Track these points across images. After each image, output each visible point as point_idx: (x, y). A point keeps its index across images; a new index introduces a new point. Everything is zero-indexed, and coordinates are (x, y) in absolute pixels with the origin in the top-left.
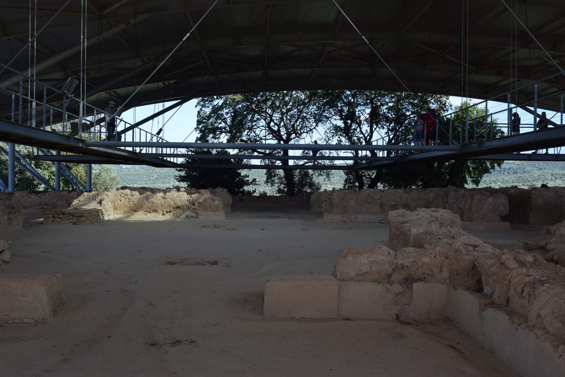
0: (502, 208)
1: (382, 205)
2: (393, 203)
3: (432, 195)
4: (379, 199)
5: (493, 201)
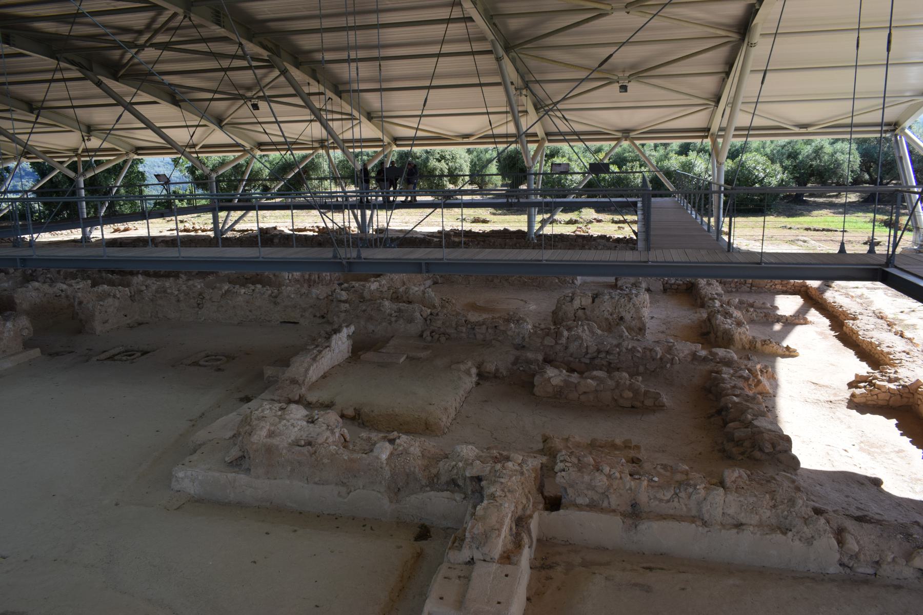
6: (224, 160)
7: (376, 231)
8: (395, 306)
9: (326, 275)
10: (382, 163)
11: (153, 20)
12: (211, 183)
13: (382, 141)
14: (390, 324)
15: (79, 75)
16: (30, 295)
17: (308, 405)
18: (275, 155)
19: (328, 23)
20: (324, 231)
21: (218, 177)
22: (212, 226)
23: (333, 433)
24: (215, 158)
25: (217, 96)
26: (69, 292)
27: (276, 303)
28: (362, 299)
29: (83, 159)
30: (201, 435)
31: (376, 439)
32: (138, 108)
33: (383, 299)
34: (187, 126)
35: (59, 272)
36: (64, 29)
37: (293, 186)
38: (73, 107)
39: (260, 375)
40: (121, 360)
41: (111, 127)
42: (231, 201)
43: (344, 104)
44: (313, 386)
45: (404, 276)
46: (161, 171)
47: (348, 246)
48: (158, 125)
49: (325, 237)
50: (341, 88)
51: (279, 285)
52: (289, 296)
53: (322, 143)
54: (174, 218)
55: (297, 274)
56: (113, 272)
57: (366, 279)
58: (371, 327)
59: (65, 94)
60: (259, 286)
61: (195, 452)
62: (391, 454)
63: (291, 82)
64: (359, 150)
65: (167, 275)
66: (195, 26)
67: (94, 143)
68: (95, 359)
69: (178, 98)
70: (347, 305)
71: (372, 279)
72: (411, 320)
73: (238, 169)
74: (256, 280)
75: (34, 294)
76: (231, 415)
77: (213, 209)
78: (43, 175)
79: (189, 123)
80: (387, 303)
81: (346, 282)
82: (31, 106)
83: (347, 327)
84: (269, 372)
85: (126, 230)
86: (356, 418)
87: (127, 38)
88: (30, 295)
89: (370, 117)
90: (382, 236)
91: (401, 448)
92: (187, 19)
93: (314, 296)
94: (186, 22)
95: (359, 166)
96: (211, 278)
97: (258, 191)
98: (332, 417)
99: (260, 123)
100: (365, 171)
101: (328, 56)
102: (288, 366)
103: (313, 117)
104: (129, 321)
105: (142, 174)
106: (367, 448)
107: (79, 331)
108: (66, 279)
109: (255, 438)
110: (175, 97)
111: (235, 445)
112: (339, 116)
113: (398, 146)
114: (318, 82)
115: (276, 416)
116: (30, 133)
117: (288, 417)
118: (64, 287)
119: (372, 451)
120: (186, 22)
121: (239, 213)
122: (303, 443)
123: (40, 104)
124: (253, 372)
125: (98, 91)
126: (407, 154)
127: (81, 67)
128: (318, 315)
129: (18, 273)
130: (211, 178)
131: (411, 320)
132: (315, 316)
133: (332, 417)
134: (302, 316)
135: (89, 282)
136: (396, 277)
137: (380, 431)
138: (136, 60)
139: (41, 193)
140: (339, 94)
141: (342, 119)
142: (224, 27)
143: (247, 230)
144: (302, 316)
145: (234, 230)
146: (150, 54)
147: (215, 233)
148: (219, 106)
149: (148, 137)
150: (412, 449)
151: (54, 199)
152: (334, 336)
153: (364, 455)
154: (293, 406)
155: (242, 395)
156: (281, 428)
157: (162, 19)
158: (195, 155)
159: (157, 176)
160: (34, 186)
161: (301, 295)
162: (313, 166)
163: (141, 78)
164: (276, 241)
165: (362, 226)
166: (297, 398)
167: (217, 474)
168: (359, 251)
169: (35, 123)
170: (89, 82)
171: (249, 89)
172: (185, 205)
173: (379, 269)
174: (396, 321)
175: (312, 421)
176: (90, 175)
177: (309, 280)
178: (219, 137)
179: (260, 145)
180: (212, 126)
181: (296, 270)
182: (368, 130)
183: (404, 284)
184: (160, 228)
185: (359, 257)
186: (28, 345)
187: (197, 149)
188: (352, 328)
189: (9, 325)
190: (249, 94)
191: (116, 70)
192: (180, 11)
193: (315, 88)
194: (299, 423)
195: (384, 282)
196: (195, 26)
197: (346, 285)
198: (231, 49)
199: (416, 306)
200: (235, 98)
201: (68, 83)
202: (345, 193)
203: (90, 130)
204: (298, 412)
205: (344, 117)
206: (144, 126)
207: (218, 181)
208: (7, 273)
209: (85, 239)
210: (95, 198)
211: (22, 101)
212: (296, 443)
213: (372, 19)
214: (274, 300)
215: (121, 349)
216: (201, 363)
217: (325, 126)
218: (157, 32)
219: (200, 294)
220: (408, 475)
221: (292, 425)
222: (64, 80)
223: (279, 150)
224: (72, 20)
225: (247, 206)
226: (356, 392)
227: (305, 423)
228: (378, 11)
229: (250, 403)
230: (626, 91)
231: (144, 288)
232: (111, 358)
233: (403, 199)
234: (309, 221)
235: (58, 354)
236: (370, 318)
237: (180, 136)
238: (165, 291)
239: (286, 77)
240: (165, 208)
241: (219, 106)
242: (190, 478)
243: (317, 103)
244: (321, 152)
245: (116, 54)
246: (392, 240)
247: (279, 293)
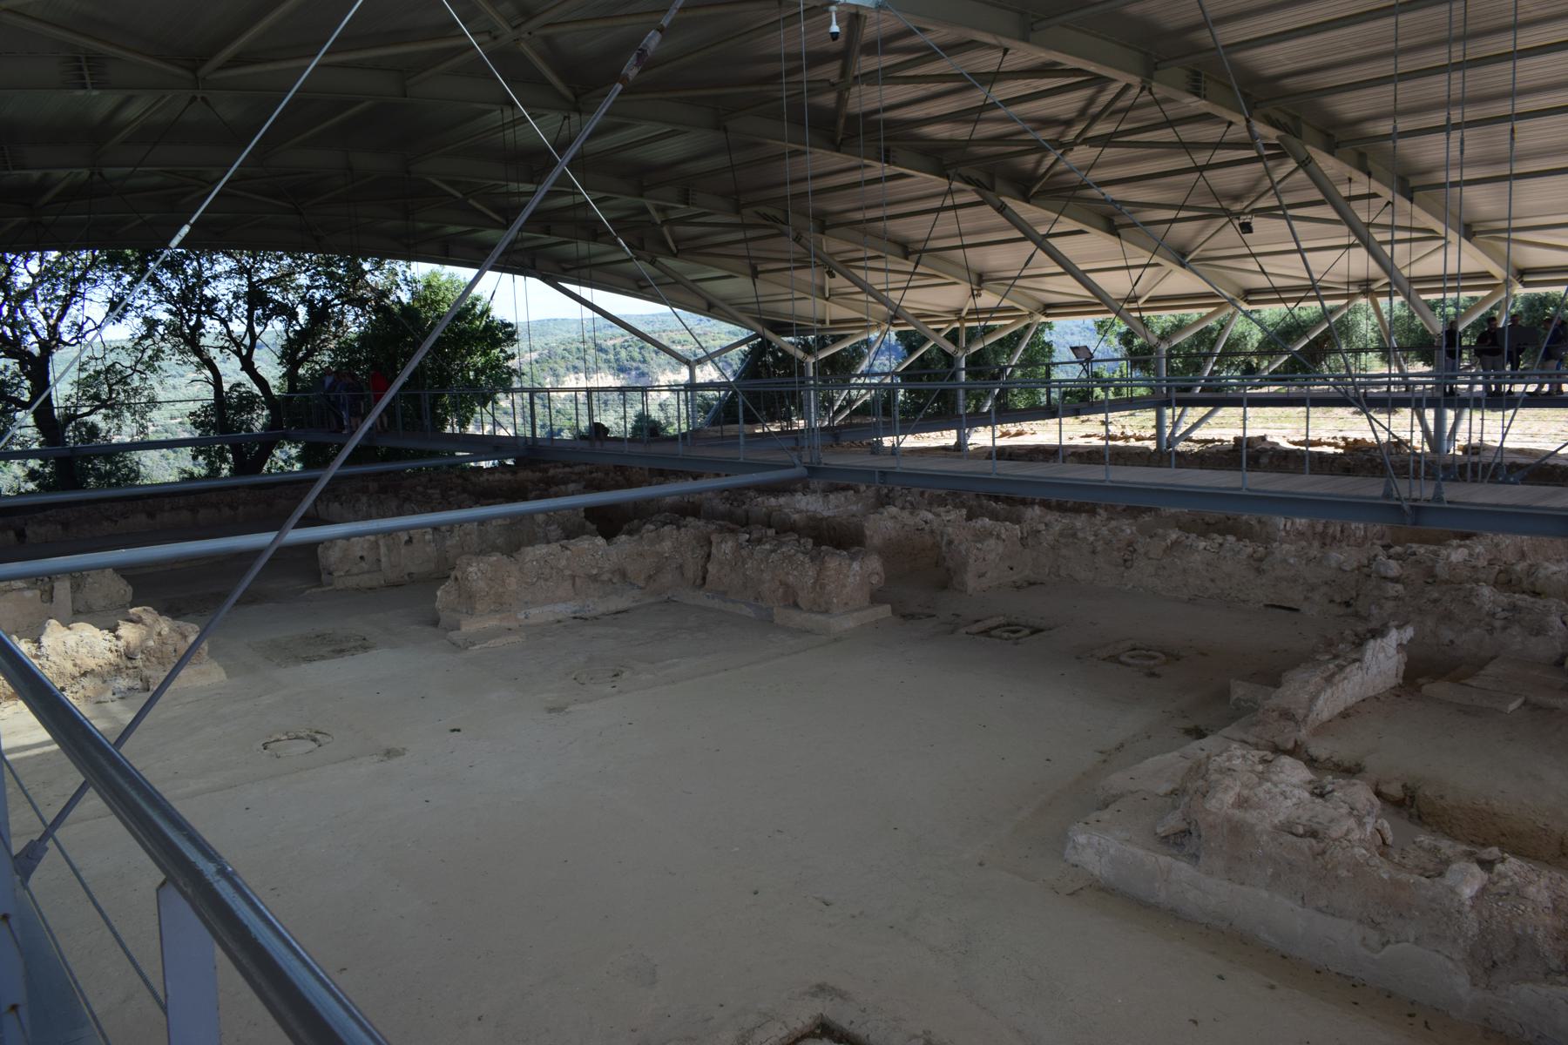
6: (1181, 321)
7: (1465, 449)
8: (1504, 598)
9: (1358, 527)
10: (1490, 319)
11: (1091, 101)
12: (1158, 360)
13: (1491, 276)
14: (1491, 630)
15: (975, 198)
16: (884, 524)
17: (1311, 762)
18: (1272, 312)
19: (1528, 39)
20: (1354, 447)
21: (1169, 350)
22: (1154, 431)
23: (1361, 824)
24: (1166, 318)
25: (1183, 214)
26: (935, 525)
27: (1259, 571)
28: (1431, 577)
29: (967, 325)
30: (1117, 780)
31: (1449, 852)
32: (1055, 242)
33: (1477, 581)
34: (1128, 268)
35: (922, 494)
36: (961, 132)
37: (1303, 361)
38: (963, 247)
39: (1224, 694)
40: (1000, 637)
41: (1016, 274)
42: (1188, 389)
43: (1417, 210)
44: (1323, 729)
45: (1525, 541)
46: (1078, 341)
47: (1416, 476)
48: (1082, 267)
49: (1357, 458)
50: (1413, 182)
51: (1268, 540)
52: (1285, 561)
53: (1366, 287)
55: (1301, 522)
56: (997, 499)
57: (1441, 540)
58: (1447, 634)
59: (954, 228)
60: (1231, 538)
61: (1107, 806)
62: (1483, 890)
63: (1318, 180)
64: (1440, 296)
65: (1077, 509)
66: (1157, 102)
67: (988, 299)
68: (963, 631)
69: (1117, 221)
70: (1399, 587)
71: (1455, 542)
72: (1539, 630)
73: (1206, 338)
74: (1226, 527)
75: (890, 524)
76: (1169, 756)
77: (1157, 403)
78: (911, 349)
79: (1131, 263)
80: (1486, 591)
81: (1398, 542)
82: (906, 249)
83: (1398, 627)
84: (1240, 690)
85: (1019, 434)
86: (1406, 804)
87: (1046, 135)
88: (884, 524)
89: (1469, 231)
90: (1475, 459)
91: (1506, 883)
92: (1145, 92)
93: (1334, 564)
94: (1145, 97)
95: (1438, 326)
96: (1147, 518)
97: (1238, 374)
98: (1361, 793)
99: (1253, 255)
100: (1451, 333)
101: (1385, 127)
102: (1277, 685)
103: (1353, 239)
104: (1015, 578)
105: (1049, 345)
106: (1431, 866)
107: (944, 585)
108: (930, 504)
109: (1212, 804)
110: (1112, 222)
111: (1176, 808)
112: (1406, 235)
113: (1526, 285)
114: (1369, 175)
115: (1252, 771)
116: (906, 288)
117: (1275, 778)
118: (930, 516)
119: (1441, 874)
120: (1145, 97)
121: (1202, 411)
122: (1301, 830)
123: (921, 246)
124: (1214, 686)
125: (1000, 219)
126: (1544, 301)
127: (977, 185)
128: (1338, 599)
129: (871, 493)
130: (1158, 352)
131: (1539, 630)
132: (1332, 601)
133: (1361, 793)
134: (1306, 598)
135: (964, 512)
136: (1506, 541)
137: (1455, 838)
138: (1058, 168)
139: (908, 376)
140: (1409, 193)
141: (1411, 240)
142: (1205, 97)
143: (1213, 441)
144: (1306, 598)
145: (1191, 440)
146: (1082, 154)
147: (1159, 444)
148: (1182, 231)
149: (1068, 287)
150: (1532, 890)
151: (925, 385)
152: (1372, 643)
153: (1423, 879)
154: (1286, 760)
155: (1190, 724)
156: (1262, 795)
157: (1105, 98)
158: (1136, 314)
159: (1074, 349)
160: (900, 365)
161: (1309, 561)
162: (1345, 328)
163: (1064, 194)
164: (1264, 460)
165: (1436, 439)
166: (1290, 745)
167: (1141, 853)
168: (1438, 487)
169: (912, 274)
170: (988, 208)
171: (1237, 198)
172: (1111, 396)
173: (1468, 524)
174: (1504, 628)
175: (1320, 793)
176: (973, 349)
177: (1323, 535)
178: (1181, 281)
179: (1248, 294)
180: (1168, 265)
181: (1301, 516)
182: (1472, 259)
183: (1523, 556)
184: (1077, 432)
185: (1438, 498)
186: (876, 598)
187: (1141, 302)
188: (1409, 632)
189: (856, 566)
190: (1237, 207)
191: (1026, 186)
192: (1135, 80)
193: (1361, 185)
194: (1296, 792)
195: (1479, 549)
196: (1157, 102)
197: (1398, 549)
198: (1210, 133)
199: (1553, 603)
200: (1211, 215)
201: (960, 212)
202: (1405, 376)
203: (980, 280)
204: (1293, 773)
205: (1415, 235)
206: (1060, 270)
207: (1170, 356)
208: (857, 491)
209: (960, 446)
210: (979, 385)
211: (895, 242)
212: (1288, 828)
213: (1503, 43)
214: (1257, 565)
215: (1002, 620)
216: (1123, 659)
217: (1373, 251)
218: (1095, 119)
219: (1130, 544)
220: (1517, 940)
221: (1283, 793)
222: (955, 207)
223: (1283, 301)
224: (975, 117)
225: (1217, 398)
226: (1406, 752)
227: (1307, 795)
228: (1516, 26)
229: (1203, 742)
230: (1250, 231)
231: (1042, 527)
232: (986, 632)
233: (1532, 388)
234: (1336, 427)
235: (912, 616)
236: (1447, 617)
237: (1116, 284)
238: (1074, 535)
239: (1307, 172)
240: (1079, 402)
241: (1182, 231)
242: (1098, 847)
243: (1362, 213)
244: (1363, 301)
245: (1029, 161)
246: (1514, 467)
247: (1267, 555)
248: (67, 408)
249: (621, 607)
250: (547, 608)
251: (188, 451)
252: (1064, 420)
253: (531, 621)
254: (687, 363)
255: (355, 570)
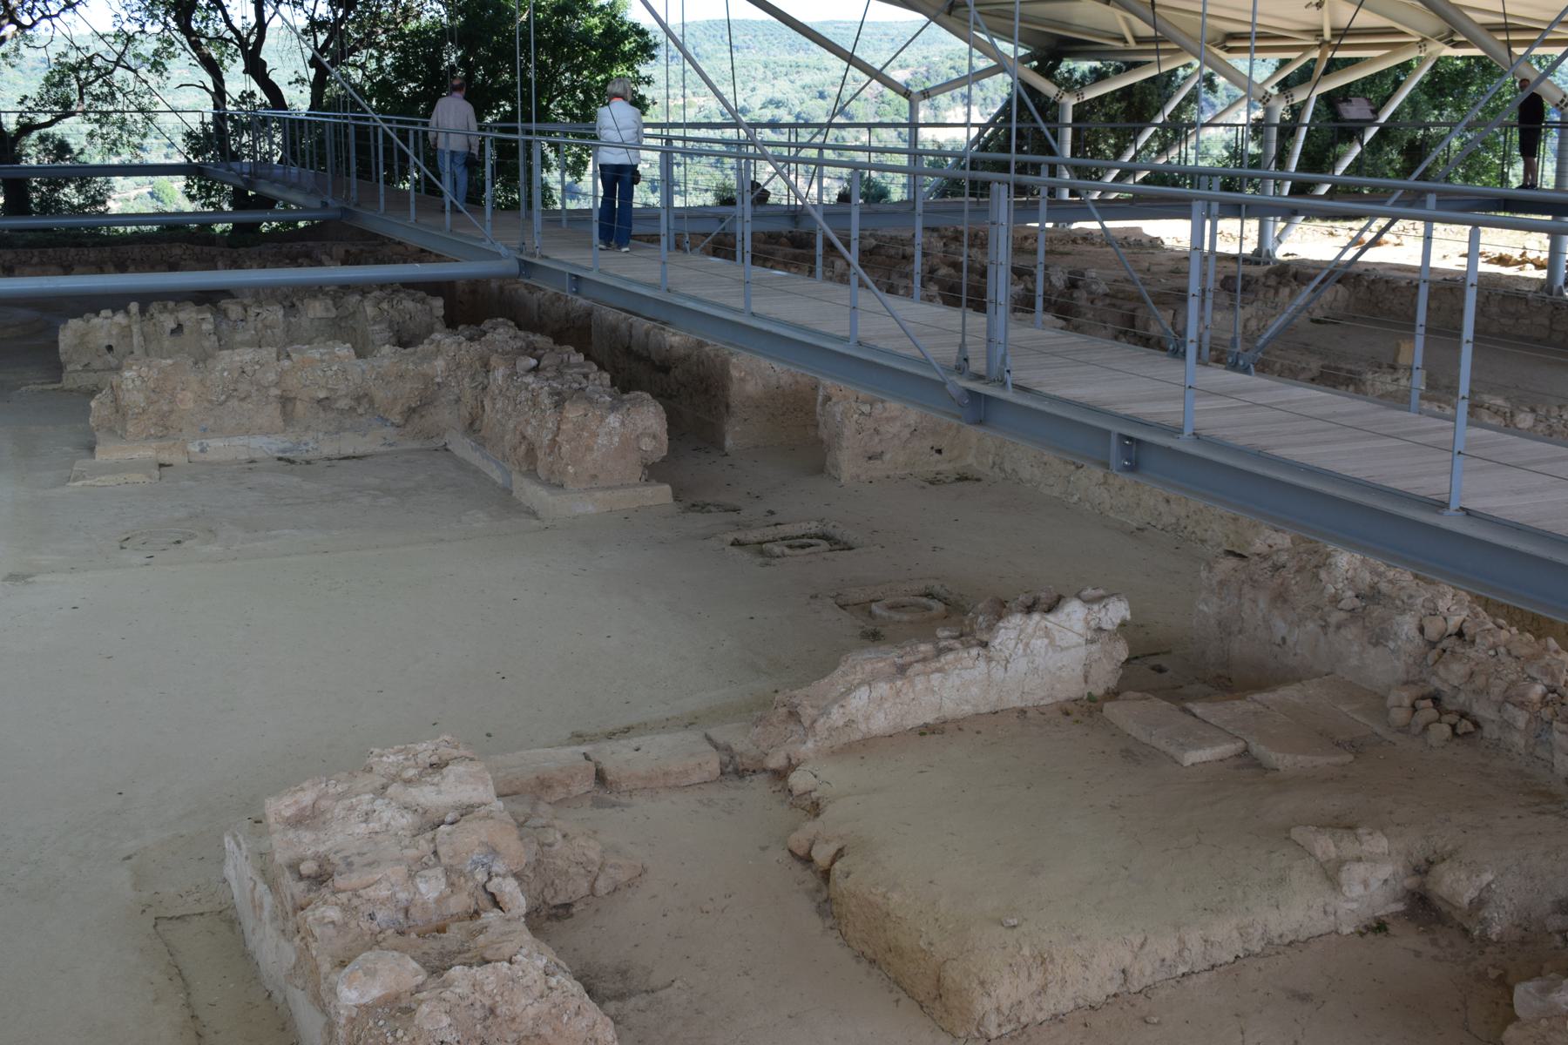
0: (647, 444)
1: (286, 401)
2: (322, 395)
3: (440, 363)
4: (277, 385)
5: (623, 423)
54: (1483, 267)
104: (943, 467)
152: (1017, 620)
168: (853, 327)
189: (613, 420)
248: (21, 114)
249: (360, 450)
250: (237, 441)
251: (179, 182)
252: (1438, 228)
253: (209, 457)
254: (907, 94)
255: (97, 364)
